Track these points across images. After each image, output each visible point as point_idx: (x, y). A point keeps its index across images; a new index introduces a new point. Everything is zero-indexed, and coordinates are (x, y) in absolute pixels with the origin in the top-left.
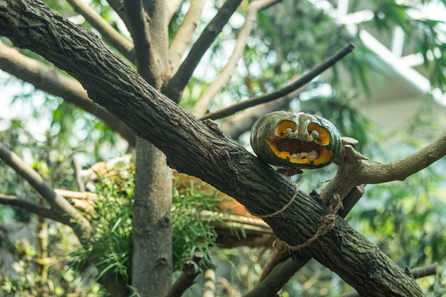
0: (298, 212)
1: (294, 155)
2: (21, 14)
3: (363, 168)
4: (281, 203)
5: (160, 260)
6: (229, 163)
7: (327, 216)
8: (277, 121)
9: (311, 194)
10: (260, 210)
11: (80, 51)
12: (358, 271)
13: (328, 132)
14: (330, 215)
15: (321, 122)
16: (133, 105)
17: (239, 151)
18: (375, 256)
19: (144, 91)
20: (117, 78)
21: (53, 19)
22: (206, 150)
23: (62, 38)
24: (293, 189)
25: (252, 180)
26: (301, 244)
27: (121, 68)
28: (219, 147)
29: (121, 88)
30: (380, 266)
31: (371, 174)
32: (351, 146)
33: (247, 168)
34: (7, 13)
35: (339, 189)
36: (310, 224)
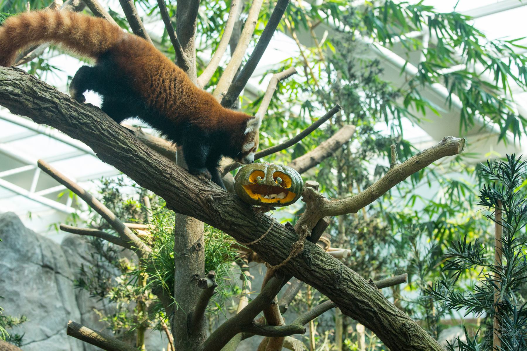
1: (266, 197)
2: (34, 98)
3: (324, 204)
5: (194, 276)
6: (213, 205)
7: (297, 242)
8: (251, 171)
9: (286, 225)
11: (85, 124)
12: (327, 284)
13: (291, 178)
15: (285, 171)
16: (133, 164)
18: (340, 272)
19: (141, 153)
20: (118, 143)
21: (62, 100)
23: (70, 114)
24: (270, 222)
25: (234, 217)
30: (345, 279)
34: (21, 98)
36: (284, 248)
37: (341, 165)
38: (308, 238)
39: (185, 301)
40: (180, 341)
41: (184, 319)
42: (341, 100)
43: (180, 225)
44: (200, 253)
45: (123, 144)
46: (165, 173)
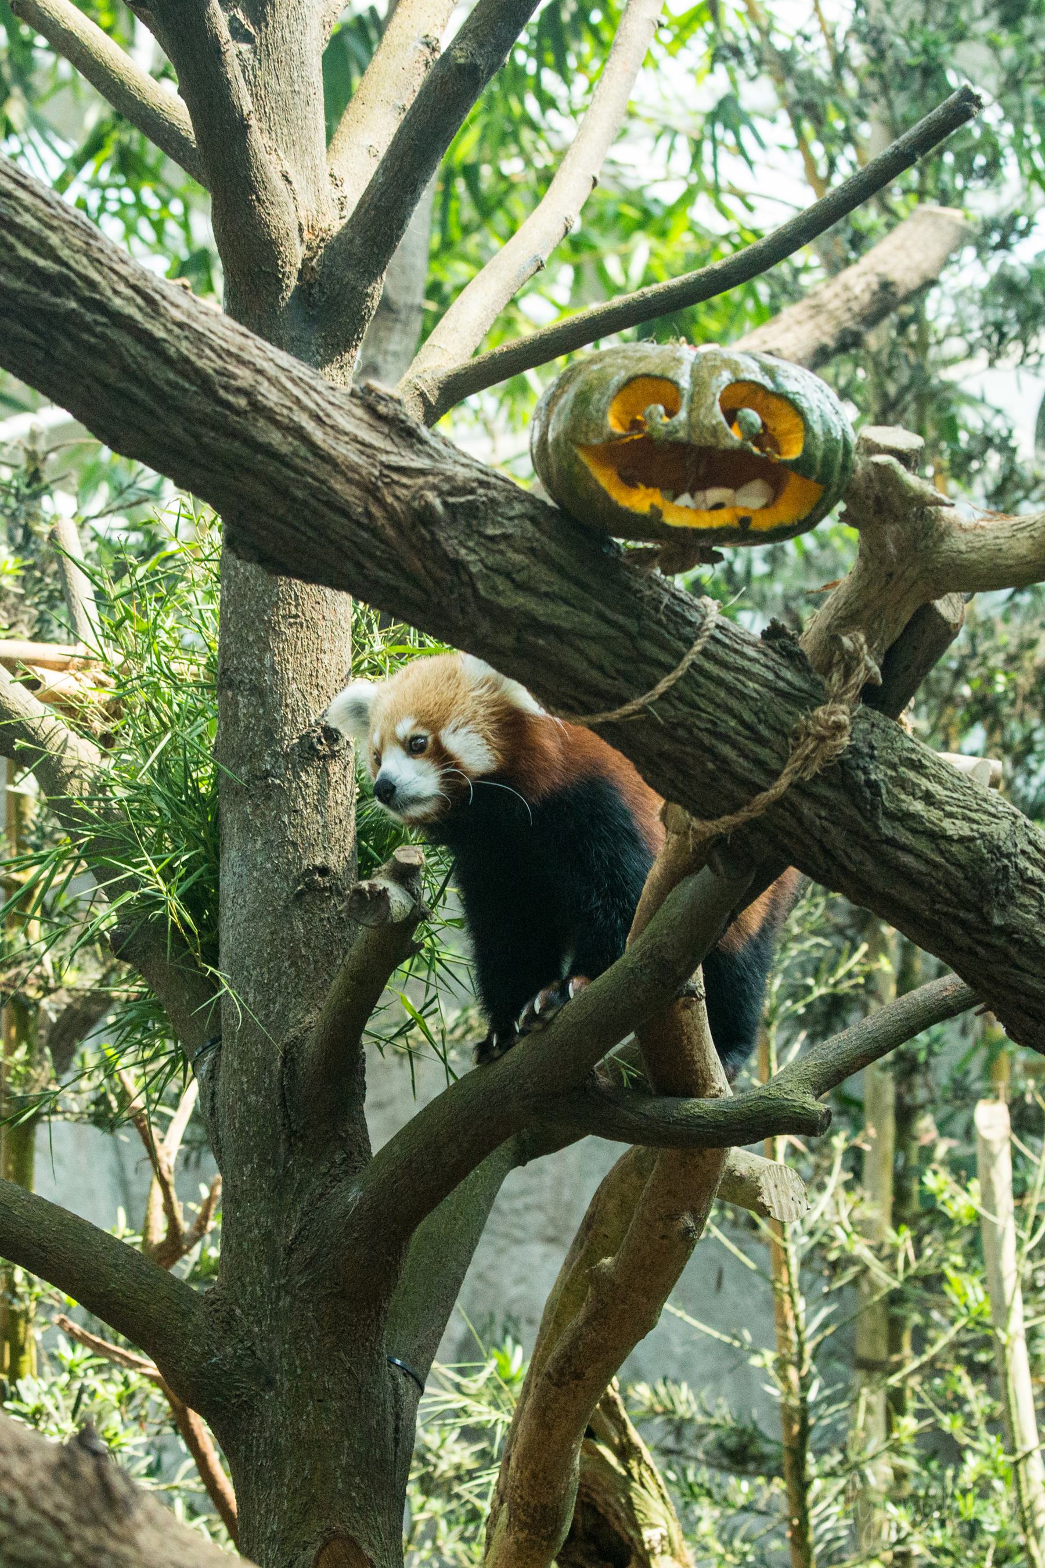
0: (712, 701)
1: (685, 499)
4: (649, 669)
5: (308, 873)
6: (441, 536)
7: (819, 712)
10: (575, 698)
12: (947, 902)
13: (800, 413)
14: (828, 707)
15: (773, 379)
16: (78, 343)
17: (481, 491)
19: (116, 292)
20: (11, 248)
22: (358, 493)
26: (731, 813)
27: (27, 209)
28: (405, 480)
29: (28, 281)
30: (1031, 881)
31: (974, 556)
32: (893, 460)
33: (516, 551)
35: (867, 613)
36: (761, 741)
37: (892, 389)
38: (870, 694)
39: (269, 986)
40: (247, 1170)
41: (265, 1065)
42: (892, 93)
43: (241, 639)
44: (335, 768)
45: (36, 252)
46: (226, 388)
